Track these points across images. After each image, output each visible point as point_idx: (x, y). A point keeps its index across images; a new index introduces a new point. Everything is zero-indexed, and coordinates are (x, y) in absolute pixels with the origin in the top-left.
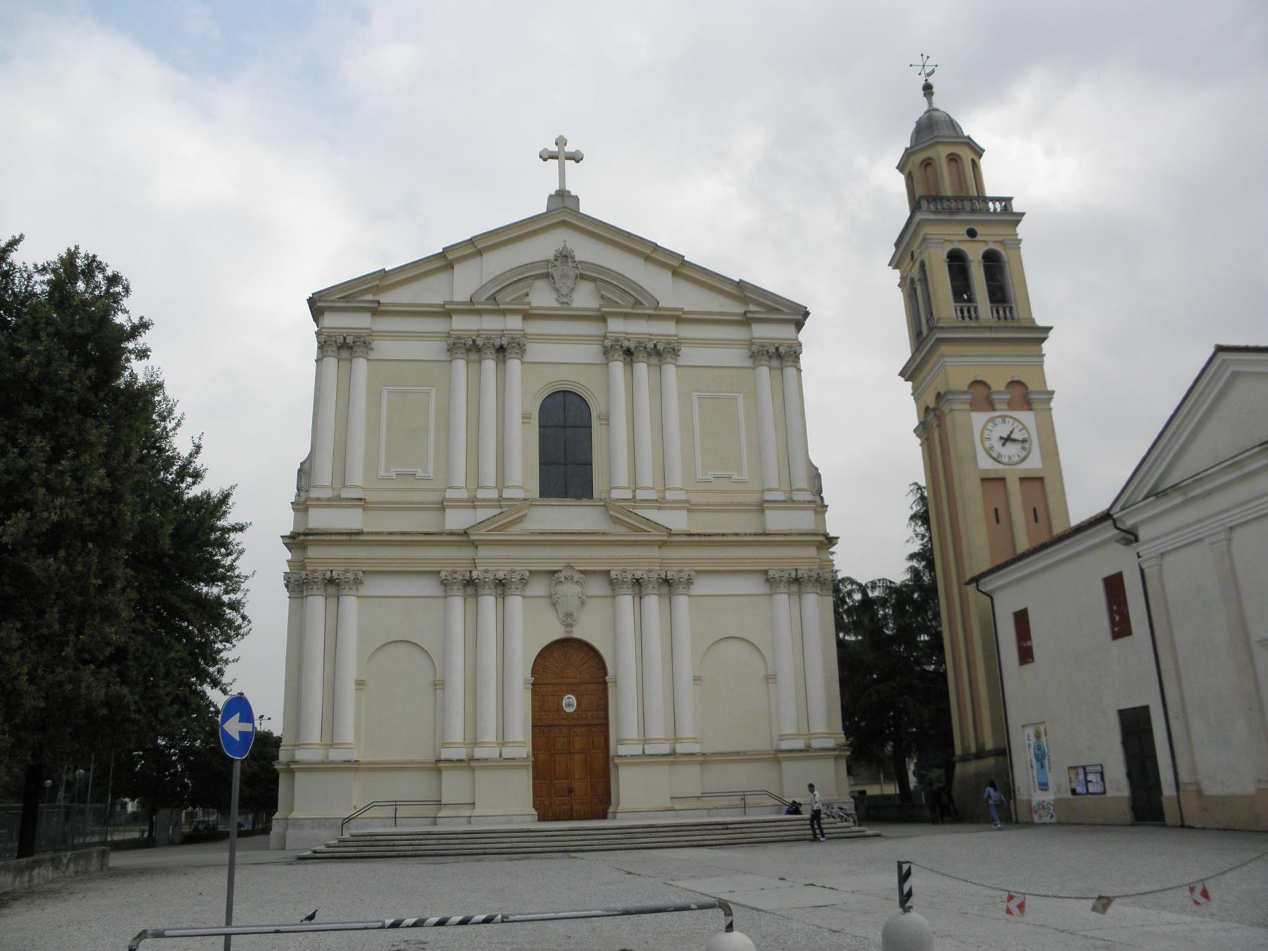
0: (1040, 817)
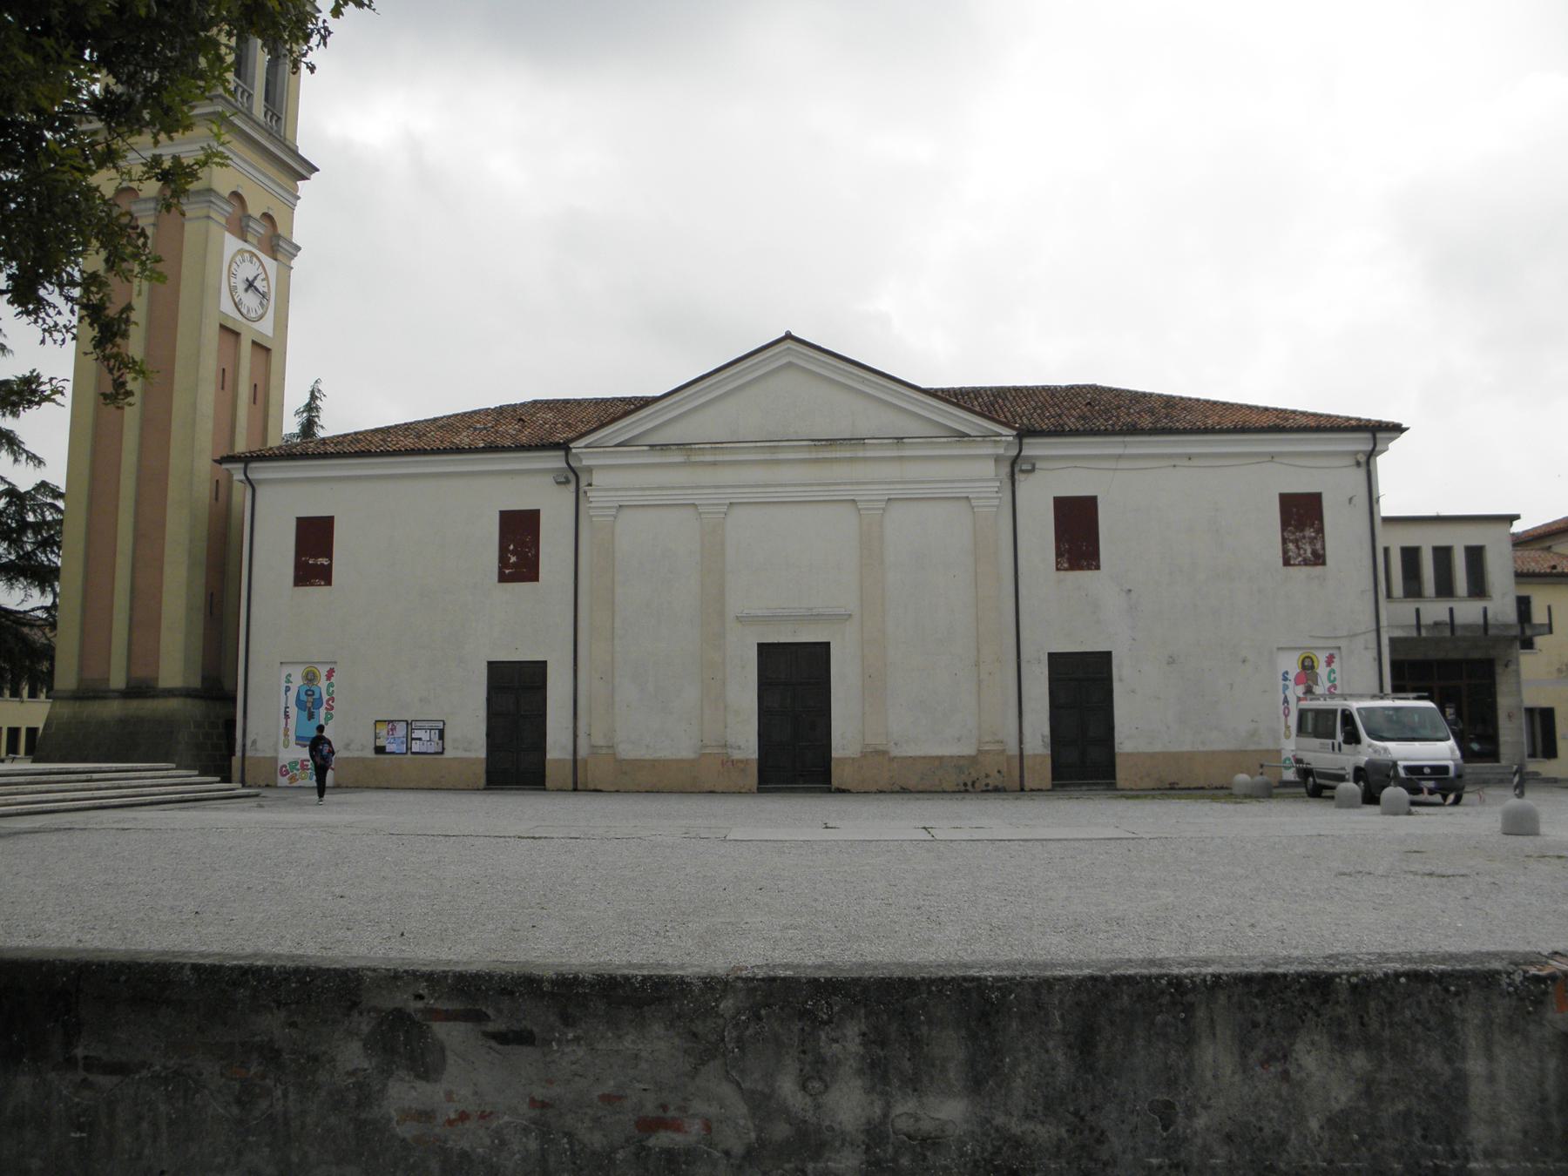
0: (293, 779)
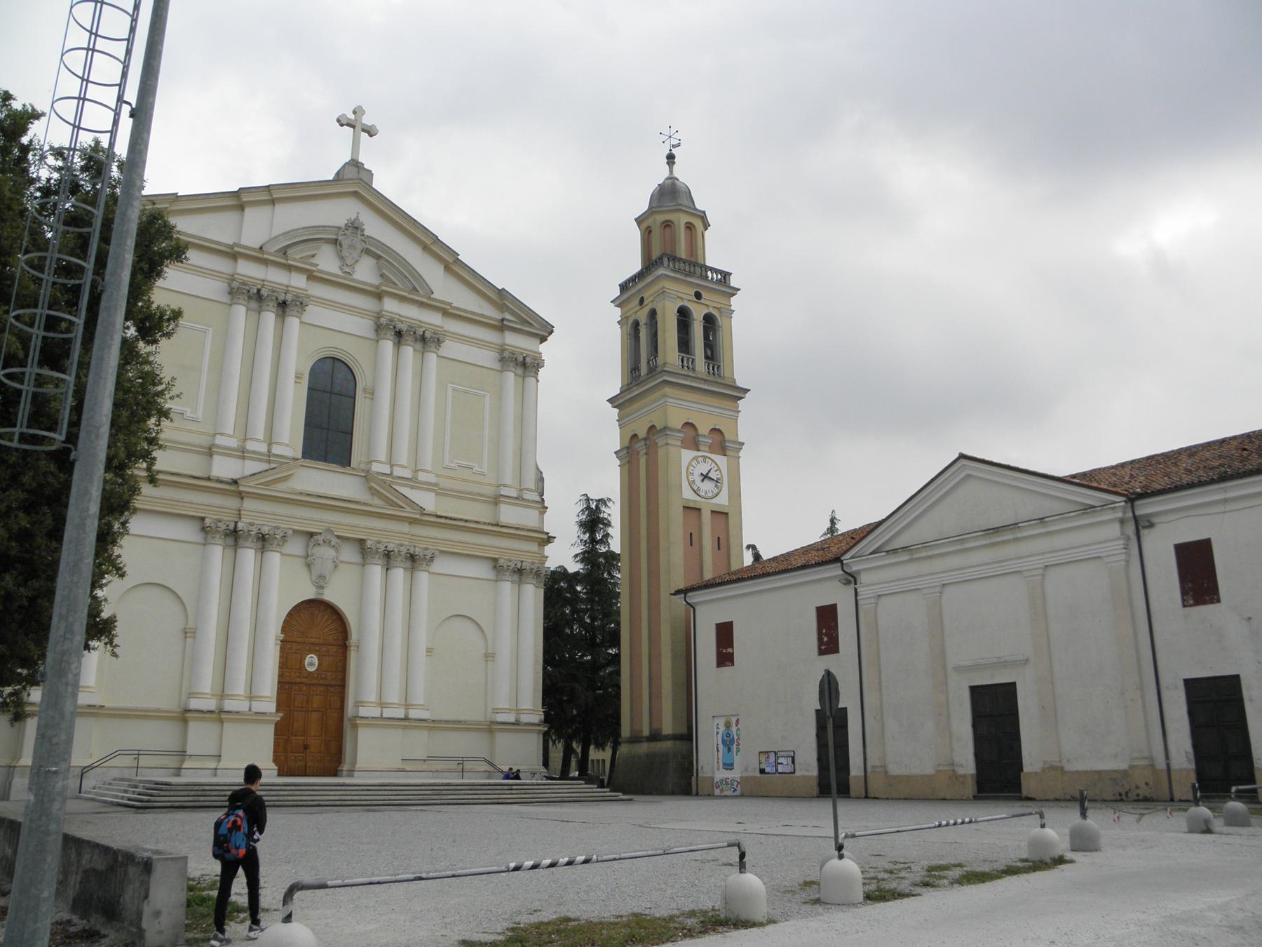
0: (722, 791)
